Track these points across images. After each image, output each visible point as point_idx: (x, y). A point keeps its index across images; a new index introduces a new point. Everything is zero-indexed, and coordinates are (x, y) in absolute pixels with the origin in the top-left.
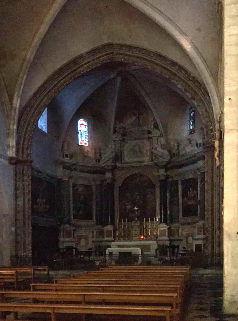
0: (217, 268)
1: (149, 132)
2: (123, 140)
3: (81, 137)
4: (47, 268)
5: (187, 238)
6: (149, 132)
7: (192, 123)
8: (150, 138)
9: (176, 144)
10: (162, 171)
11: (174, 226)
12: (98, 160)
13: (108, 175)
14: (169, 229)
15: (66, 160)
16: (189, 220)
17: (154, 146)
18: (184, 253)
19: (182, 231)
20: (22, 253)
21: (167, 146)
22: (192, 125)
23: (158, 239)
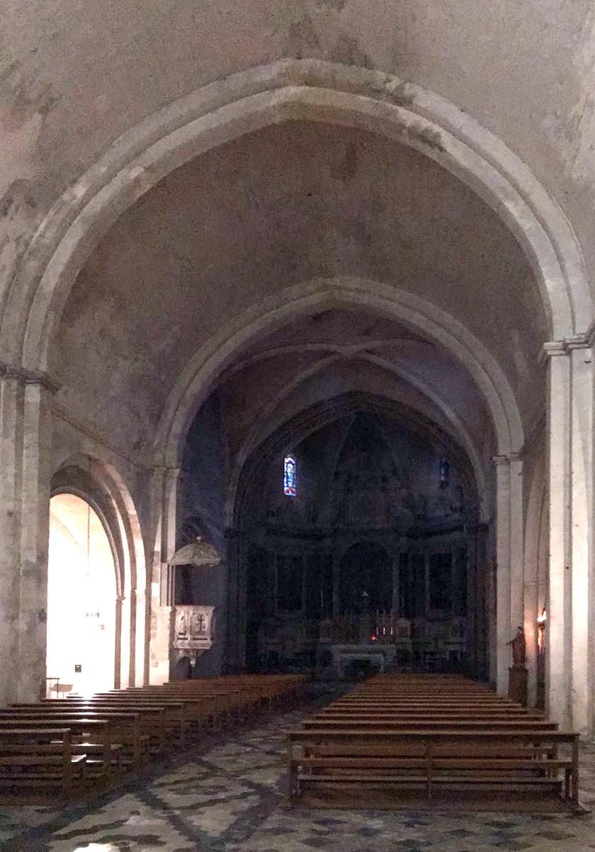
0: (547, 314)
1: (384, 480)
2: (349, 490)
3: (287, 483)
4: (444, 657)
5: (436, 640)
6: (384, 480)
7: (443, 472)
8: (384, 489)
9: (423, 503)
10: (403, 540)
11: (419, 621)
12: (314, 520)
13: (327, 542)
14: (412, 626)
15: (271, 520)
16: (440, 613)
17: (299, 358)
18: (91, 747)
19: (429, 632)
20: (232, 661)
21: (407, 502)
22: (444, 475)
23: (396, 642)
